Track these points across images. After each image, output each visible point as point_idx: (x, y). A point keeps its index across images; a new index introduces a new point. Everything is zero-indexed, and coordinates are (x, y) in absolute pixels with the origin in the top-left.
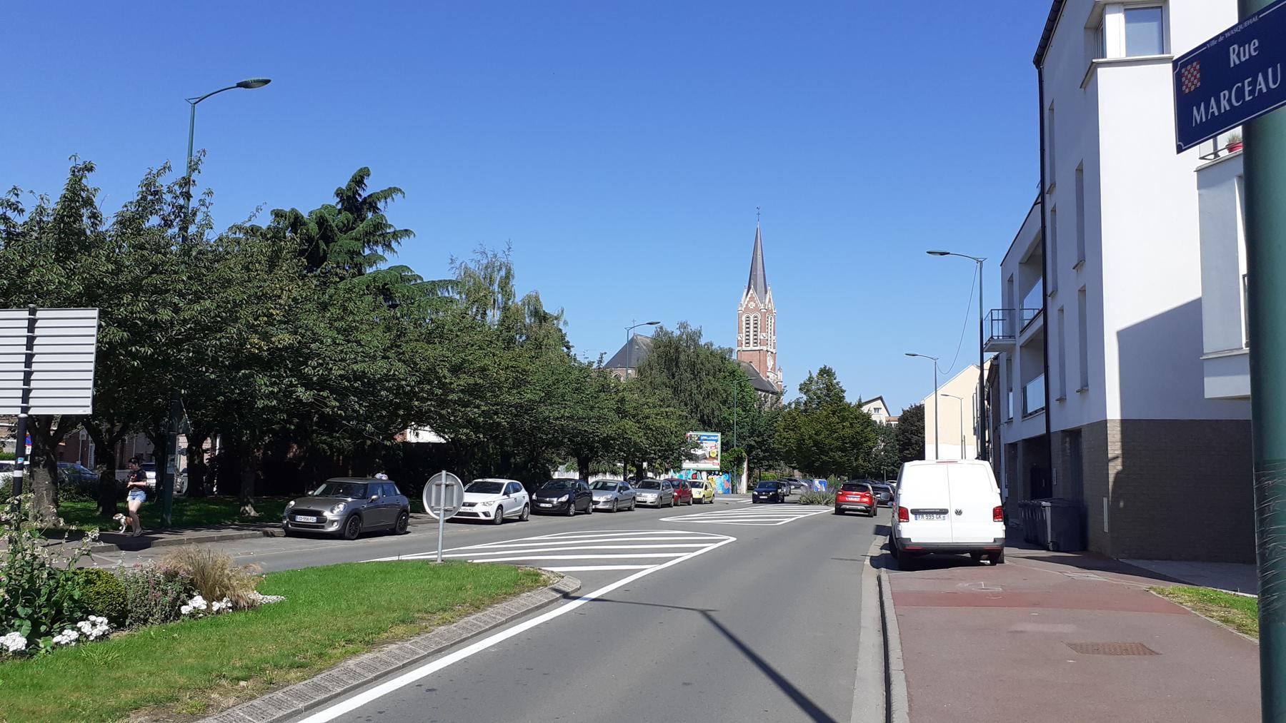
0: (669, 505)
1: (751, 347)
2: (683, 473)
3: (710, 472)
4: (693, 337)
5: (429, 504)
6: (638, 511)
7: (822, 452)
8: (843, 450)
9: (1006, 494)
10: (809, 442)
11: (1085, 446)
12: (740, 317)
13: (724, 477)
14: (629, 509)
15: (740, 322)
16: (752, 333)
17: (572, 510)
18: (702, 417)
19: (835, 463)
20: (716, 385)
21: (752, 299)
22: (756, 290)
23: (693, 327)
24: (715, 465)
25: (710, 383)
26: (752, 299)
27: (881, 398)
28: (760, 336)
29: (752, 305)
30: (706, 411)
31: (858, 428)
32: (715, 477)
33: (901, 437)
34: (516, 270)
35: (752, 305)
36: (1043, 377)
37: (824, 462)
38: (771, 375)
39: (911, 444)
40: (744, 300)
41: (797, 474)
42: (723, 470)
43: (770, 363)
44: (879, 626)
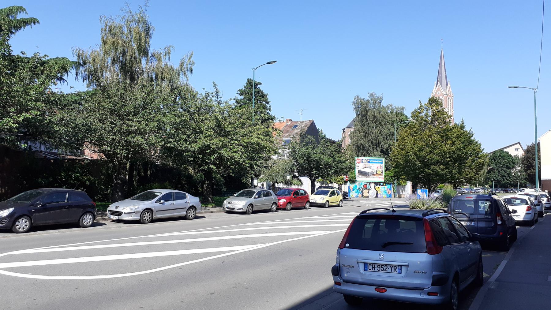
2: (357, 184)
3: (376, 184)
4: (377, 101)
5: (19, 199)
6: (313, 209)
7: (427, 166)
8: (446, 164)
9: (68, 98)
10: (413, 157)
13: (387, 187)
17: (289, 207)
18: (382, 150)
19: (436, 174)
20: (392, 130)
21: (439, 89)
22: (441, 84)
23: (378, 95)
24: (381, 179)
25: (387, 128)
26: (439, 89)
27: (519, 143)
30: (385, 146)
31: (458, 144)
33: (525, 162)
34: (151, 22)
37: (429, 174)
42: (387, 183)
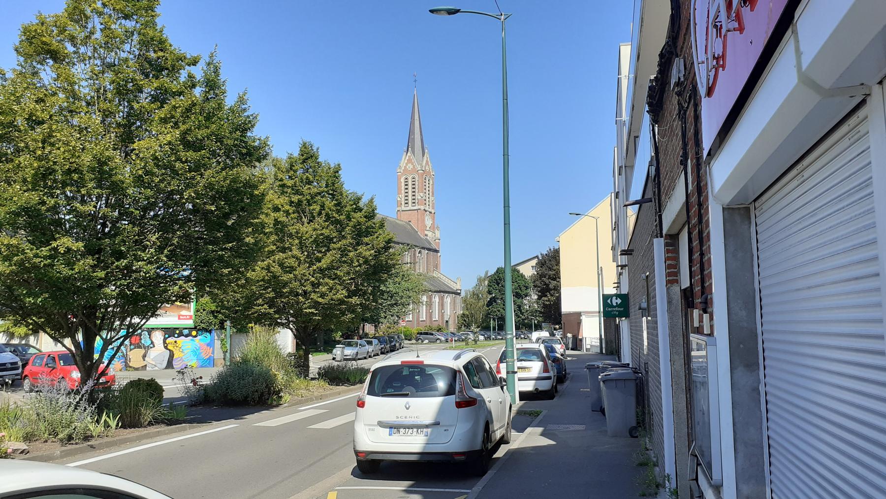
0: (378, 355)
1: (410, 207)
11: (872, 230)
12: (399, 178)
14: (365, 358)
15: (399, 183)
16: (410, 194)
21: (409, 161)
22: (413, 152)
28: (418, 197)
29: (410, 167)
32: (181, 340)
33: (538, 283)
35: (410, 167)
36: (804, 66)
38: (430, 234)
39: (549, 290)
40: (403, 163)
41: (136, 320)
43: (428, 222)
44: (644, 24)
